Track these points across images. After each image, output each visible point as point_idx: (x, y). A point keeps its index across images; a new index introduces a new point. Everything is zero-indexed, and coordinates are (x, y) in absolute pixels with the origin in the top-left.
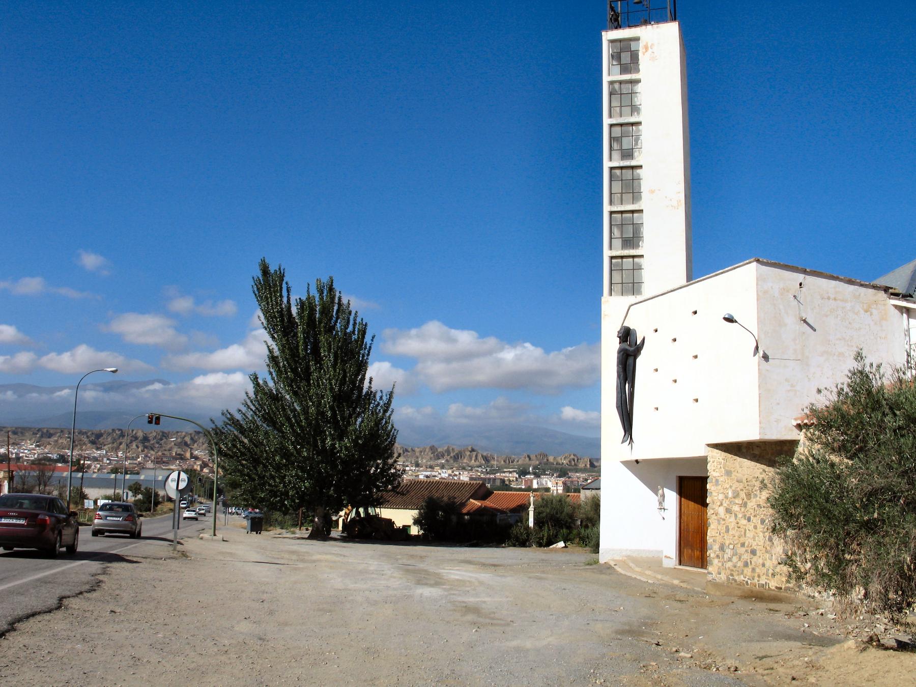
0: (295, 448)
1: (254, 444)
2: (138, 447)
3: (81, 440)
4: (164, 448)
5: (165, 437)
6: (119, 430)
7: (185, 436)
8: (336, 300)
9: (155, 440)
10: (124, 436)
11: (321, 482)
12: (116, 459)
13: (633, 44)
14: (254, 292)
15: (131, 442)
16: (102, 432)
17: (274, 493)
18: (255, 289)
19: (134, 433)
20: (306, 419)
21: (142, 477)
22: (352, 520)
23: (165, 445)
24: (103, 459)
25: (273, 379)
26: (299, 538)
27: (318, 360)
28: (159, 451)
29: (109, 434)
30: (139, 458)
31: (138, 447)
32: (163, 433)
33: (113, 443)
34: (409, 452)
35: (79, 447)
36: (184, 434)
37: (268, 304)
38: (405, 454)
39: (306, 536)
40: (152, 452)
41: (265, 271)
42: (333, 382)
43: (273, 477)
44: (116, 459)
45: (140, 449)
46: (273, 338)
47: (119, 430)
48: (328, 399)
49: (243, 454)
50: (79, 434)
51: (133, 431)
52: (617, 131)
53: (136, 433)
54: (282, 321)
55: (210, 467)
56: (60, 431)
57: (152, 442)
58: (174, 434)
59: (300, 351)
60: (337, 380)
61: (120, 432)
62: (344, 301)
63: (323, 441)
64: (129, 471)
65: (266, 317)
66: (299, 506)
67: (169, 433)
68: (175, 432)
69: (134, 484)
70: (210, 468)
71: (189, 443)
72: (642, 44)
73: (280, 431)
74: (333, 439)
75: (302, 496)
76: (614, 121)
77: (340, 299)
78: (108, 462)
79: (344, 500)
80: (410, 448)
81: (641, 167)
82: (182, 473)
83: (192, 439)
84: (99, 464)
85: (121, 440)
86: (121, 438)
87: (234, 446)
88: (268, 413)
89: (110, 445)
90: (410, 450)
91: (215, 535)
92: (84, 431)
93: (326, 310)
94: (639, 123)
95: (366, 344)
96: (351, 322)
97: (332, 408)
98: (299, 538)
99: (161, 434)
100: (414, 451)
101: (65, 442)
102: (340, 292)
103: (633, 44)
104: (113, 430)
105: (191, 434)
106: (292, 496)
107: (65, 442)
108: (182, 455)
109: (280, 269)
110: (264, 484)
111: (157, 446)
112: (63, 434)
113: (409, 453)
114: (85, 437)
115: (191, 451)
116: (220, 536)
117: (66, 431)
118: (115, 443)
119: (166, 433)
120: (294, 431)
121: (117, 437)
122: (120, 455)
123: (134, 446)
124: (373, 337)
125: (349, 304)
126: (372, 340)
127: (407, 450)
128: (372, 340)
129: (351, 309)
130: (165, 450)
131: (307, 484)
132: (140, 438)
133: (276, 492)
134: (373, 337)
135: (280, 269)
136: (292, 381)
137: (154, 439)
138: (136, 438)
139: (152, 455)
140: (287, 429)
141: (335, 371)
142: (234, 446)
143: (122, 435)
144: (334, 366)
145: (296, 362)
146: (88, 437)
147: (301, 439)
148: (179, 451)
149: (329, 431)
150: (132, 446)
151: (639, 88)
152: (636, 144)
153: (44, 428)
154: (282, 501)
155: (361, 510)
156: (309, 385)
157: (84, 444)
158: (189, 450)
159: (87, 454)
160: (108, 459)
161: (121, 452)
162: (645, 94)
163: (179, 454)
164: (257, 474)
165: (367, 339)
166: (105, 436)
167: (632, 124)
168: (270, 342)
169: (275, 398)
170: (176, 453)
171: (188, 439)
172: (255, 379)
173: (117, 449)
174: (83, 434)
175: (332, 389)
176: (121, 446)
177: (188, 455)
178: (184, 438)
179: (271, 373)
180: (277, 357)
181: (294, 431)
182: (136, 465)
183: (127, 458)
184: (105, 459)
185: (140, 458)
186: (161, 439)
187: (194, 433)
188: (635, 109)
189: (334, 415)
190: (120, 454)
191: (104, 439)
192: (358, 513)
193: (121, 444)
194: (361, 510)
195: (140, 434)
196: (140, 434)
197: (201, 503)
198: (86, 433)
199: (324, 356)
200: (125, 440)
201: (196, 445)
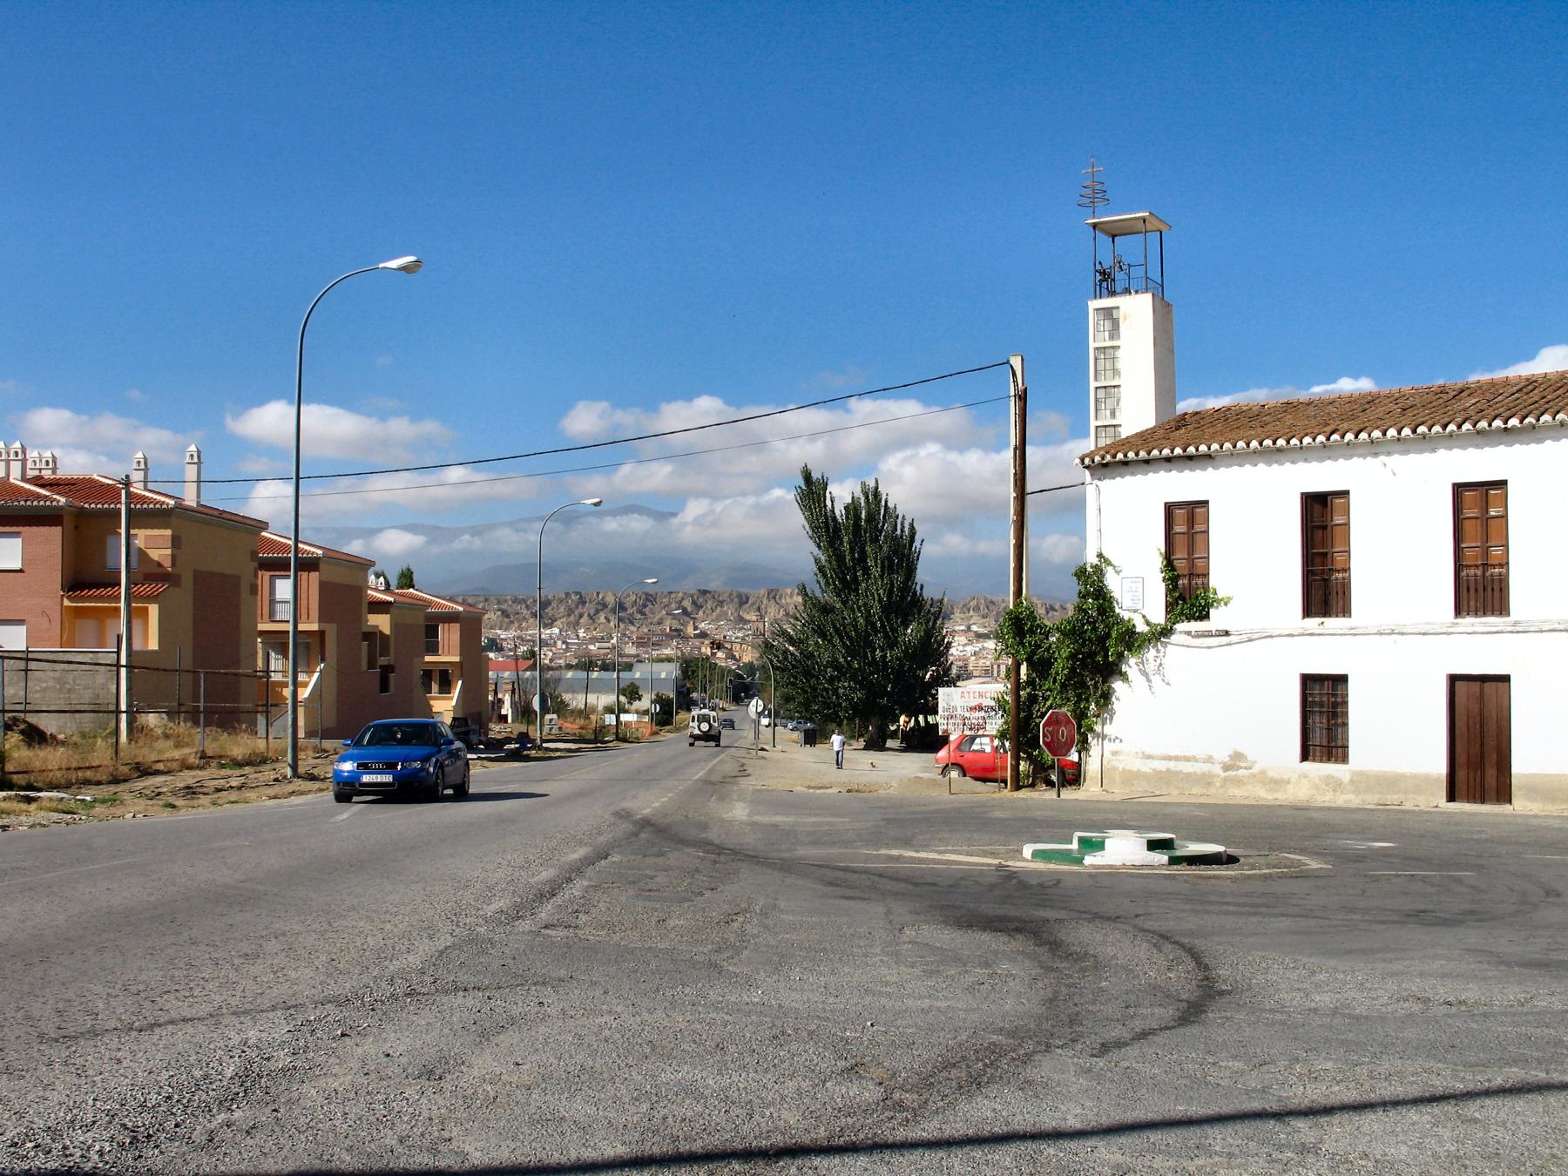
0: (846, 659)
1: (805, 656)
2: (608, 621)
3: (518, 614)
4: (649, 621)
5: (652, 601)
6: (577, 593)
7: (683, 599)
8: (883, 503)
9: (635, 608)
10: (584, 603)
11: (874, 692)
12: (577, 641)
13: (1114, 311)
14: (797, 501)
15: (597, 612)
16: (550, 597)
17: (827, 705)
18: (799, 499)
19: (600, 596)
20: (856, 631)
21: (637, 675)
22: (911, 729)
23: (651, 616)
24: (555, 643)
25: (821, 587)
26: (855, 749)
27: (866, 571)
28: (642, 625)
29: (561, 601)
30: (612, 638)
31: (608, 621)
32: (647, 594)
33: (569, 615)
34: (1056, 611)
35: (516, 625)
36: (680, 595)
37: (812, 514)
38: (1050, 615)
39: (862, 747)
40: (632, 628)
41: (807, 476)
42: (881, 591)
43: (826, 690)
44: (577, 641)
45: (612, 624)
46: (819, 547)
47: (577, 593)
48: (876, 609)
49: (794, 667)
50: (513, 602)
51: (598, 594)
52: (1101, 394)
53: (603, 598)
54: (827, 531)
55: (727, 648)
56: (483, 599)
57: (631, 611)
58: (665, 597)
59: (847, 561)
60: (885, 590)
61: (578, 596)
62: (891, 505)
63: (873, 652)
64: (599, 660)
65: (810, 527)
66: (854, 716)
67: (657, 594)
68: (666, 593)
69: (628, 686)
70: (726, 651)
71: (689, 609)
72: (1122, 312)
73: (830, 641)
74: (882, 650)
75: (854, 706)
76: (1098, 384)
77: (886, 502)
78: (564, 646)
79: (896, 710)
80: (1058, 604)
81: (1120, 425)
82: (759, 701)
83: (694, 603)
84: (551, 650)
85: (580, 610)
86: (580, 606)
87: (786, 659)
88: (818, 626)
89: (565, 619)
90: (1057, 607)
91: (774, 747)
92: (521, 597)
93: (871, 518)
94: (1118, 386)
95: (916, 548)
96: (899, 527)
97: (880, 619)
98: (855, 749)
99: (643, 597)
100: (1065, 609)
101: (494, 618)
102: (887, 495)
103: (1114, 311)
104: (567, 594)
105: (692, 596)
106: (846, 707)
107: (494, 618)
108: (681, 630)
109: (823, 477)
110: (817, 697)
111: (639, 616)
112: (489, 605)
113: (1055, 613)
114: (523, 606)
115: (694, 623)
116: (779, 747)
117: (492, 599)
118: (573, 616)
119: (651, 595)
120: (844, 644)
121: (573, 605)
122: (581, 635)
123: (602, 620)
124: (922, 541)
125: (895, 508)
126: (921, 545)
127: (1053, 609)
128: (921, 545)
129: (898, 512)
130: (651, 623)
131: (859, 695)
132: (610, 606)
133: (829, 704)
134: (922, 541)
135: (823, 477)
136: (840, 591)
137: (633, 607)
138: (605, 606)
139: (632, 632)
140: (836, 640)
141: (883, 581)
142: (786, 659)
143: (582, 601)
144: (882, 577)
145: (843, 572)
146: (528, 607)
147: (851, 652)
148: (676, 625)
149: (879, 640)
150: (599, 618)
151: (1119, 353)
152: (1118, 404)
153: (458, 596)
154: (836, 713)
155: (921, 718)
156: (858, 594)
157: (525, 619)
158: (692, 623)
159: (530, 635)
160: (563, 643)
161: (583, 630)
162: (1124, 359)
163: (676, 630)
164: (810, 687)
165: (917, 543)
166: (554, 605)
167: (1115, 387)
168: (816, 551)
169: (826, 609)
170: (670, 628)
171: (687, 604)
172: (803, 590)
173: (576, 625)
174: (520, 603)
175: (880, 600)
176: (582, 621)
177: (690, 631)
178: (681, 602)
179: (818, 582)
180: (824, 567)
181: (844, 644)
182: (608, 651)
183: (594, 640)
184: (559, 643)
185: (615, 639)
186: (645, 606)
187: (697, 593)
188: (1116, 372)
189: (883, 626)
190: (581, 633)
191: (553, 609)
192: (917, 722)
193: (581, 616)
194: (921, 718)
195: (610, 599)
196: (610, 599)
197: (1513, 904)
198: (524, 601)
199: (871, 566)
200: (589, 608)
201: (701, 613)
